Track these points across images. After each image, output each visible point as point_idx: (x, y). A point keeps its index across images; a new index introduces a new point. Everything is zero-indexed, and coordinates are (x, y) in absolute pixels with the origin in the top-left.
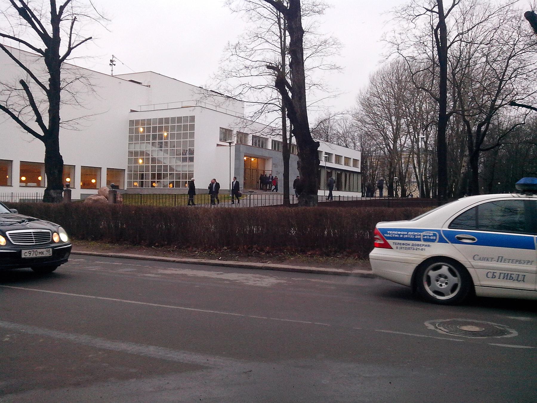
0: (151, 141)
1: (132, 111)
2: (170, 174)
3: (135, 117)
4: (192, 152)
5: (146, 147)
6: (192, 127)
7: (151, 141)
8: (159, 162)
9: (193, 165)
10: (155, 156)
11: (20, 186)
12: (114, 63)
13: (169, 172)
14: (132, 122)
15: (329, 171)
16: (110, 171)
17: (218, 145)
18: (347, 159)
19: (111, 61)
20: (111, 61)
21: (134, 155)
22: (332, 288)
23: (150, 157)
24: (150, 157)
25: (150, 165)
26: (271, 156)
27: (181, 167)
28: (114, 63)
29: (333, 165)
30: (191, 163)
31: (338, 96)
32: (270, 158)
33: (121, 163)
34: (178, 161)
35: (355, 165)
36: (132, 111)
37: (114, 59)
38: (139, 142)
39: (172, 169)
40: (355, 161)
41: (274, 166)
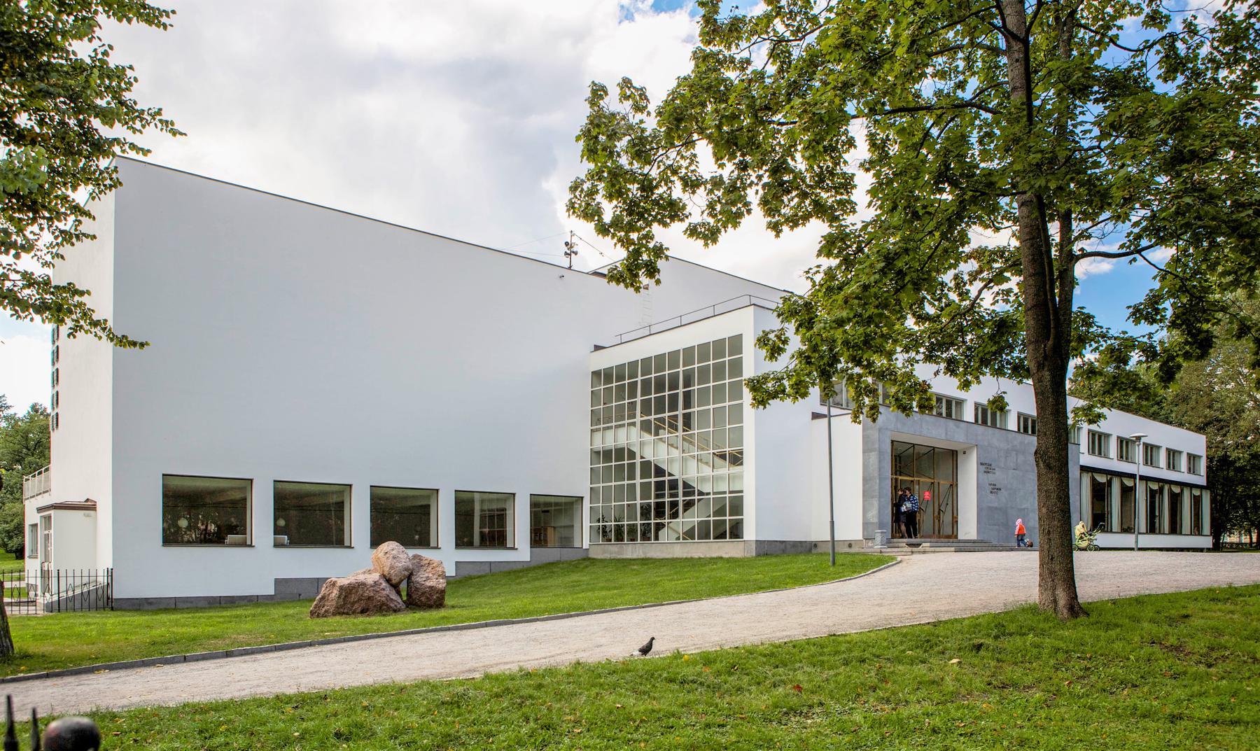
0: (638, 419)
1: (597, 348)
3: (605, 361)
5: (628, 436)
7: (638, 419)
8: (660, 472)
9: (740, 477)
10: (649, 456)
11: (276, 545)
14: (596, 374)
15: (1155, 487)
16: (649, 539)
18: (1172, 454)
19: (567, 244)
20: (567, 244)
21: (613, 461)
22: (1234, 539)
23: (638, 460)
24: (638, 460)
29: (1138, 467)
30: (736, 469)
32: (971, 448)
33: (571, 476)
35: (1192, 470)
36: (597, 348)
37: (575, 240)
38: (614, 424)
40: (1192, 458)
41: (983, 468)
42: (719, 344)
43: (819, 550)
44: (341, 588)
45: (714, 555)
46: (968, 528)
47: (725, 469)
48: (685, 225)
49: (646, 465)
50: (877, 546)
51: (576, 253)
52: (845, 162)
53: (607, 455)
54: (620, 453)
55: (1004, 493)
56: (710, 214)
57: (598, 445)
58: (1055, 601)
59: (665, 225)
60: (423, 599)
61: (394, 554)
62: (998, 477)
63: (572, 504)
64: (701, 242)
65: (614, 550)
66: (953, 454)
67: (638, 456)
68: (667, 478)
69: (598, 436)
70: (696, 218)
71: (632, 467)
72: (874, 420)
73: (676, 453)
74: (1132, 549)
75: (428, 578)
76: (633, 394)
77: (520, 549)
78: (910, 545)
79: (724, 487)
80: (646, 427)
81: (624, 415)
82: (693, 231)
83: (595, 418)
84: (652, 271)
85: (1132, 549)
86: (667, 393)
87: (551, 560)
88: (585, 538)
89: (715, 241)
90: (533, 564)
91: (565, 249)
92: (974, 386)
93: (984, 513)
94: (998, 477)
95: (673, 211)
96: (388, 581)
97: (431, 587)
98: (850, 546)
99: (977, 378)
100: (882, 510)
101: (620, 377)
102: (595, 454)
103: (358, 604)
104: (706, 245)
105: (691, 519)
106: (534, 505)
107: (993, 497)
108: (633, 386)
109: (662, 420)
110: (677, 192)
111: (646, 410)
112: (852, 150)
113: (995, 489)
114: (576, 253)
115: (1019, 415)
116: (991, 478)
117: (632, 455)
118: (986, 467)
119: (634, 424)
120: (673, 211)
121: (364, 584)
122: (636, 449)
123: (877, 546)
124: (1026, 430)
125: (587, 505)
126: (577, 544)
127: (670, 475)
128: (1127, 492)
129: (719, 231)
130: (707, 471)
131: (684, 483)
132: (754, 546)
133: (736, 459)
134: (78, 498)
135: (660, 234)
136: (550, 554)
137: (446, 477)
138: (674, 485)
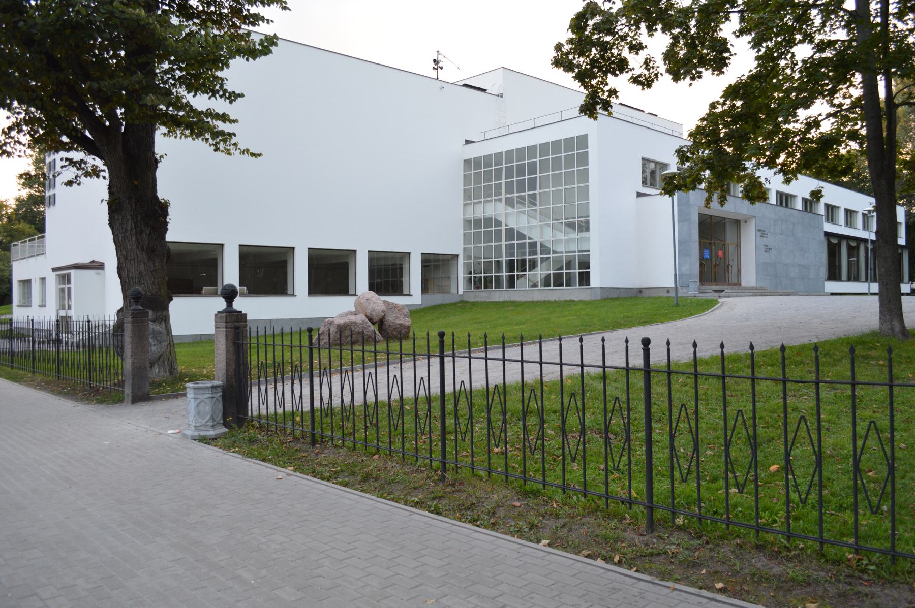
0: (503, 196)
1: (468, 142)
2: (561, 268)
3: (473, 152)
4: (588, 222)
5: (495, 209)
6: (584, 159)
7: (503, 196)
8: (521, 236)
9: (588, 239)
10: (512, 224)
12: (440, 65)
13: (564, 271)
14: (467, 162)
16: (561, 285)
17: (640, 195)
19: (435, 61)
20: (435, 61)
21: (479, 228)
23: (503, 227)
24: (503, 227)
25: (504, 243)
26: (753, 214)
27: (562, 243)
28: (440, 65)
30: (584, 235)
31: (491, 385)
33: (449, 242)
34: (558, 233)
35: (866, 227)
36: (468, 142)
37: (440, 58)
38: (483, 200)
39: (545, 250)
41: (759, 234)
42: (569, 142)
43: (643, 295)
44: (338, 326)
45: (568, 299)
46: (749, 277)
47: (575, 235)
48: (630, 75)
49: (510, 233)
50: (693, 290)
51: (441, 68)
52: (721, 30)
53: (477, 223)
54: (488, 221)
55: (773, 252)
56: (646, 68)
57: (470, 216)
58: (892, 329)
59: (616, 75)
60: (394, 333)
61: (379, 302)
62: (769, 240)
63: (448, 260)
64: (640, 87)
65: (483, 295)
66: (737, 223)
67: (503, 224)
68: (527, 241)
69: (470, 209)
70: (637, 72)
71: (498, 232)
72: (722, 205)
73: (535, 222)
74: (866, 294)
75: (397, 318)
76: (499, 177)
77: (414, 296)
78: (716, 291)
79: (574, 247)
80: (509, 202)
81: (490, 193)
82: (635, 80)
83: (467, 195)
84: (607, 105)
85: (866, 294)
86: (527, 177)
87: (437, 303)
88: (460, 286)
89: (649, 86)
90: (423, 307)
91: (433, 65)
92: (793, 182)
93: (762, 268)
94: (769, 240)
95: (622, 65)
96: (370, 320)
97: (400, 324)
98: (668, 291)
99: (796, 176)
100: (693, 266)
101: (488, 164)
102: (467, 223)
103: (346, 338)
104: (643, 89)
105: (539, 273)
106: (371, 260)
107: (766, 254)
108: (499, 171)
109: (523, 198)
110: (626, 53)
111: (509, 189)
112: (728, 23)
113: (768, 249)
114: (441, 68)
115: (778, 192)
116: (765, 241)
117: (498, 223)
118: (762, 233)
119: (500, 200)
120: (622, 65)
121: (355, 323)
122: (502, 219)
123: (693, 290)
124: (781, 204)
125: (461, 261)
126: (453, 291)
127: (530, 238)
128: (853, 251)
129: (652, 81)
130: (560, 236)
131: (541, 244)
132: (599, 292)
133: (585, 227)
134: (86, 260)
135: (613, 81)
136: (436, 299)
137: (362, 240)
138: (533, 245)
